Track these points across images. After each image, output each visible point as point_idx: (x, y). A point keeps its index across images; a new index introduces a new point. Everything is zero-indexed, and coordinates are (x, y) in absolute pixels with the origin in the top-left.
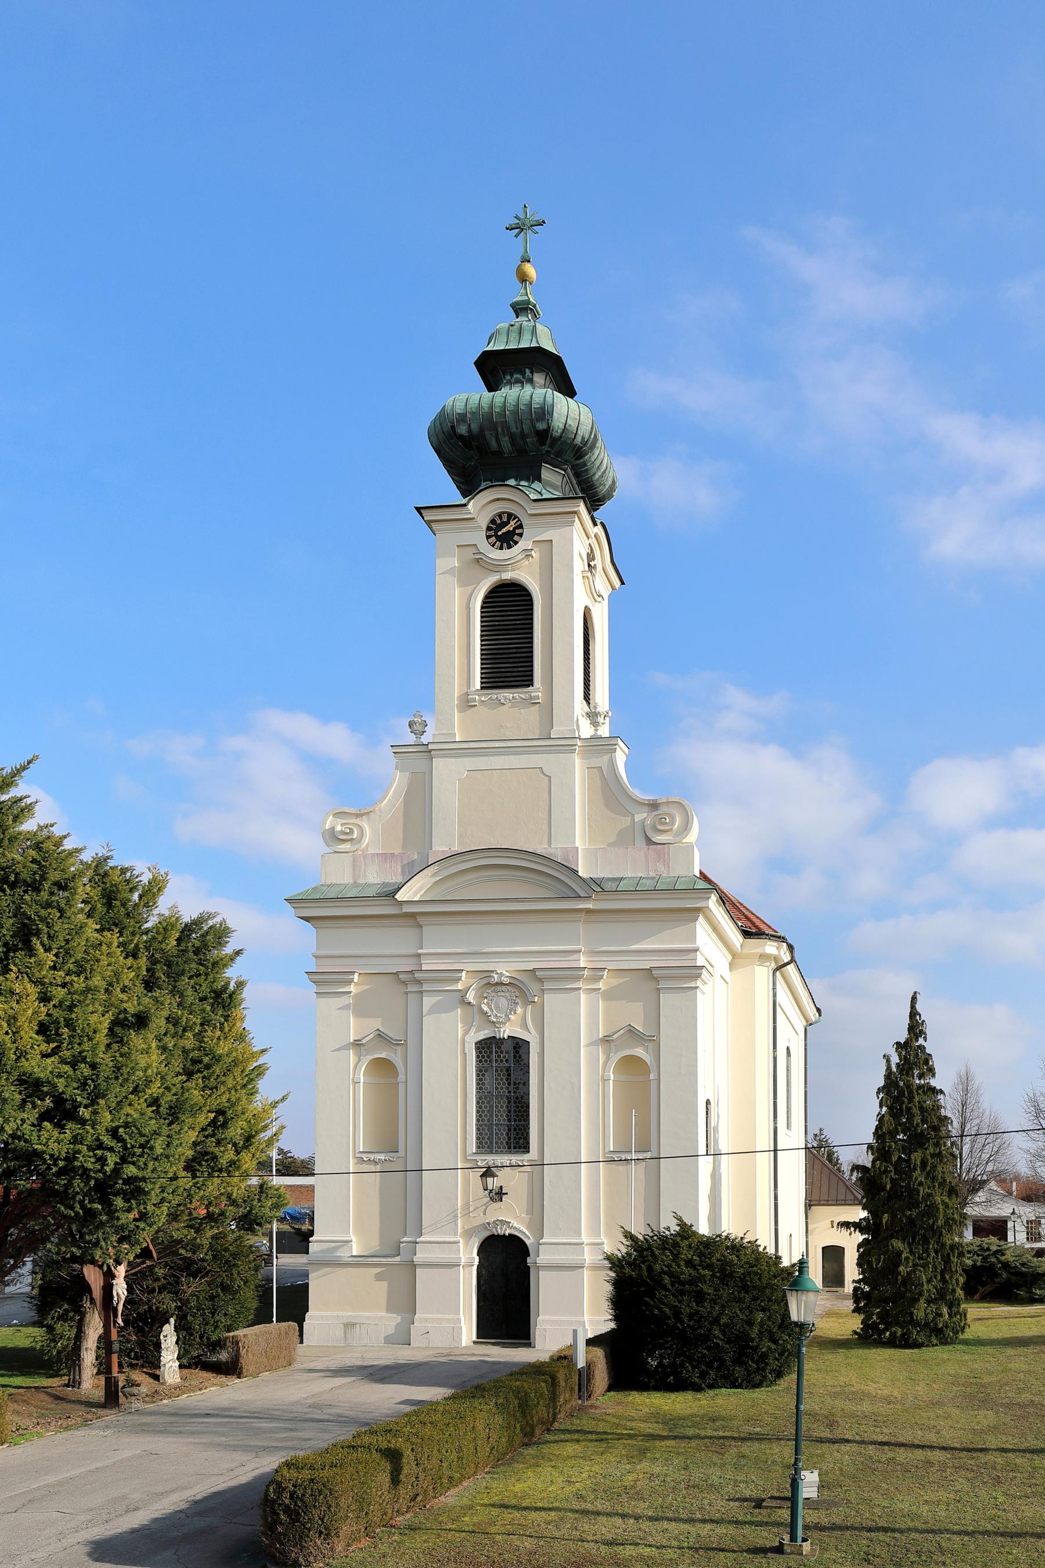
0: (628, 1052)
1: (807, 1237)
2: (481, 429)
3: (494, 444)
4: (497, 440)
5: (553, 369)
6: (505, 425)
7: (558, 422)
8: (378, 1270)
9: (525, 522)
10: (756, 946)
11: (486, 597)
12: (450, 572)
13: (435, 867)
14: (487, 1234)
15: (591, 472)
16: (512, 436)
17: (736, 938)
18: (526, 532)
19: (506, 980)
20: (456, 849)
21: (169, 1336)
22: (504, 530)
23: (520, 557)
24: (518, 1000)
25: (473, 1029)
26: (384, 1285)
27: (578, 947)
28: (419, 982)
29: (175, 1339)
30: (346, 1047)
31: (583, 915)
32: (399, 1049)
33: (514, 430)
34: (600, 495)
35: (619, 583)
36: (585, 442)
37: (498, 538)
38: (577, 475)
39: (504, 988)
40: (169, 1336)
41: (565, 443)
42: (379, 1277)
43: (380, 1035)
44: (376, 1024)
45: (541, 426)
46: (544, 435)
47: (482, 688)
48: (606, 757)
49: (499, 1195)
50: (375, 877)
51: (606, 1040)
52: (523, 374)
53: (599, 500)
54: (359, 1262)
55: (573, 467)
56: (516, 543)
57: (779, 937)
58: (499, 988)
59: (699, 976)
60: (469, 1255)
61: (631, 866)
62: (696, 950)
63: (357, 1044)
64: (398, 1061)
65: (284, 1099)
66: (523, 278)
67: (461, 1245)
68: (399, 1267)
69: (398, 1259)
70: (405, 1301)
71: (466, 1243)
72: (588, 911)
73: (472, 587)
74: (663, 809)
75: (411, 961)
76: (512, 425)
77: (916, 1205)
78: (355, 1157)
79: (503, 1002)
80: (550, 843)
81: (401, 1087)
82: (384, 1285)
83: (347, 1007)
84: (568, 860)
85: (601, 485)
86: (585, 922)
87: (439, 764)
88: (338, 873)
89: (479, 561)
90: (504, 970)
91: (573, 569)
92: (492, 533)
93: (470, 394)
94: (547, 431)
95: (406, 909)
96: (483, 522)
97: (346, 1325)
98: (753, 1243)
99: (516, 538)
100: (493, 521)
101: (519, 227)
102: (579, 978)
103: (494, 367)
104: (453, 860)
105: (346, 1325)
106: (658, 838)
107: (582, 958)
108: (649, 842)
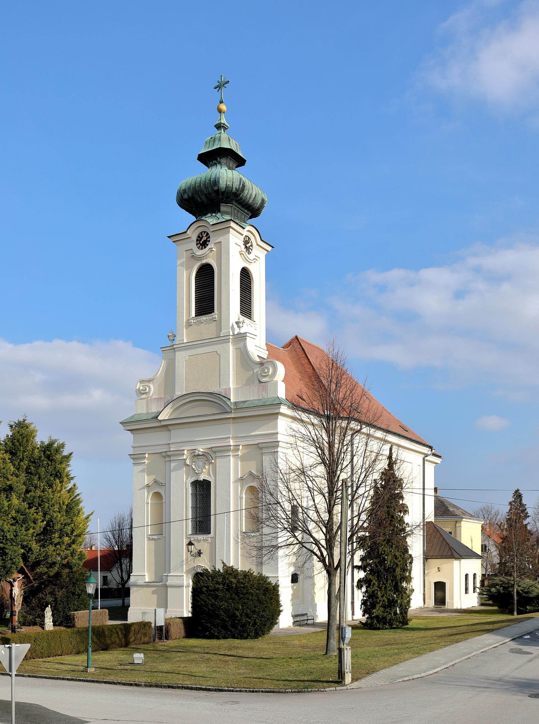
0: (252, 484)
1: (424, 576)
2: (193, 195)
3: (199, 200)
4: (200, 198)
6: (201, 191)
7: (222, 185)
8: (154, 589)
9: (210, 234)
11: (197, 273)
12: (182, 265)
13: (171, 404)
14: (194, 572)
15: (247, 201)
16: (205, 195)
18: (211, 239)
19: (200, 453)
20: (184, 393)
21: (48, 612)
22: (203, 240)
23: (208, 252)
24: (206, 462)
25: (190, 477)
26: (155, 596)
27: (230, 436)
28: (169, 456)
29: (51, 613)
30: (143, 488)
31: (231, 420)
32: (163, 487)
33: (205, 192)
34: (256, 208)
35: (271, 248)
36: (237, 190)
37: (201, 245)
38: (240, 203)
39: (201, 457)
40: (48, 612)
41: (228, 193)
42: (153, 592)
43: (156, 482)
44: (153, 477)
45: (216, 188)
46: (217, 192)
47: (196, 316)
48: (243, 343)
49: (199, 553)
50: (154, 409)
51: (242, 479)
52: (217, 160)
53: (257, 210)
54: (147, 585)
55: (236, 201)
56: (207, 245)
58: (199, 457)
59: (278, 446)
60: (188, 582)
61: (252, 395)
62: (277, 433)
63: (148, 486)
64: (163, 493)
65: (92, 513)
66: (220, 111)
67: (185, 577)
68: (161, 587)
69: (161, 583)
70: (164, 603)
71: (187, 577)
72: (234, 418)
73: (190, 270)
74: (266, 365)
75: (167, 446)
76: (204, 190)
78: (147, 537)
79: (201, 464)
80: (220, 388)
81: (164, 504)
82: (155, 596)
83: (143, 471)
84: (226, 394)
85: (254, 204)
86: (233, 423)
87: (178, 354)
88: (141, 409)
89: (194, 257)
90: (201, 449)
91: (237, 249)
92: (198, 242)
93: (202, 173)
94: (218, 190)
95: (163, 423)
96: (195, 238)
97: (143, 613)
98: (230, 572)
99: (208, 243)
100: (199, 237)
102: (230, 450)
103: (208, 158)
104: (179, 399)
105: (143, 613)
106: (264, 380)
107: (231, 441)
108: (260, 382)
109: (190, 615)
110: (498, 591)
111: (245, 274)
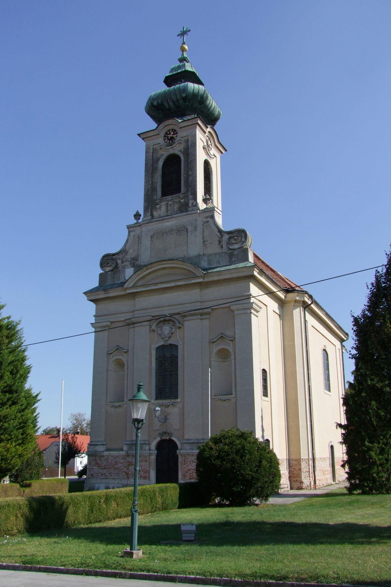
0: (221, 347)
2: (162, 101)
4: (168, 103)
5: (193, 77)
10: (291, 296)
17: (281, 295)
35: (181, 126)
45: (184, 95)
57: (303, 291)
66: (183, 50)
77: (205, 449)
96: (162, 134)
101: (183, 33)
109: (346, 423)
110: (248, 478)
111: (207, 164)
